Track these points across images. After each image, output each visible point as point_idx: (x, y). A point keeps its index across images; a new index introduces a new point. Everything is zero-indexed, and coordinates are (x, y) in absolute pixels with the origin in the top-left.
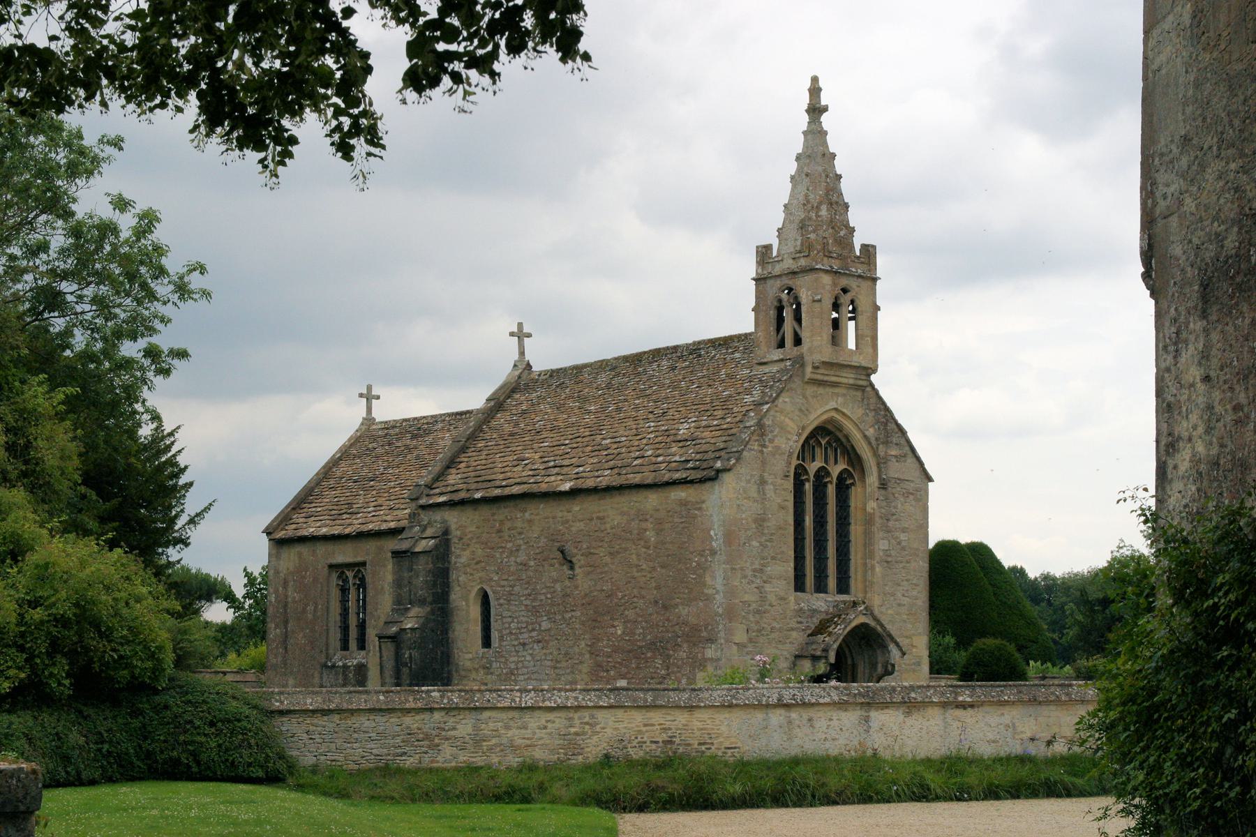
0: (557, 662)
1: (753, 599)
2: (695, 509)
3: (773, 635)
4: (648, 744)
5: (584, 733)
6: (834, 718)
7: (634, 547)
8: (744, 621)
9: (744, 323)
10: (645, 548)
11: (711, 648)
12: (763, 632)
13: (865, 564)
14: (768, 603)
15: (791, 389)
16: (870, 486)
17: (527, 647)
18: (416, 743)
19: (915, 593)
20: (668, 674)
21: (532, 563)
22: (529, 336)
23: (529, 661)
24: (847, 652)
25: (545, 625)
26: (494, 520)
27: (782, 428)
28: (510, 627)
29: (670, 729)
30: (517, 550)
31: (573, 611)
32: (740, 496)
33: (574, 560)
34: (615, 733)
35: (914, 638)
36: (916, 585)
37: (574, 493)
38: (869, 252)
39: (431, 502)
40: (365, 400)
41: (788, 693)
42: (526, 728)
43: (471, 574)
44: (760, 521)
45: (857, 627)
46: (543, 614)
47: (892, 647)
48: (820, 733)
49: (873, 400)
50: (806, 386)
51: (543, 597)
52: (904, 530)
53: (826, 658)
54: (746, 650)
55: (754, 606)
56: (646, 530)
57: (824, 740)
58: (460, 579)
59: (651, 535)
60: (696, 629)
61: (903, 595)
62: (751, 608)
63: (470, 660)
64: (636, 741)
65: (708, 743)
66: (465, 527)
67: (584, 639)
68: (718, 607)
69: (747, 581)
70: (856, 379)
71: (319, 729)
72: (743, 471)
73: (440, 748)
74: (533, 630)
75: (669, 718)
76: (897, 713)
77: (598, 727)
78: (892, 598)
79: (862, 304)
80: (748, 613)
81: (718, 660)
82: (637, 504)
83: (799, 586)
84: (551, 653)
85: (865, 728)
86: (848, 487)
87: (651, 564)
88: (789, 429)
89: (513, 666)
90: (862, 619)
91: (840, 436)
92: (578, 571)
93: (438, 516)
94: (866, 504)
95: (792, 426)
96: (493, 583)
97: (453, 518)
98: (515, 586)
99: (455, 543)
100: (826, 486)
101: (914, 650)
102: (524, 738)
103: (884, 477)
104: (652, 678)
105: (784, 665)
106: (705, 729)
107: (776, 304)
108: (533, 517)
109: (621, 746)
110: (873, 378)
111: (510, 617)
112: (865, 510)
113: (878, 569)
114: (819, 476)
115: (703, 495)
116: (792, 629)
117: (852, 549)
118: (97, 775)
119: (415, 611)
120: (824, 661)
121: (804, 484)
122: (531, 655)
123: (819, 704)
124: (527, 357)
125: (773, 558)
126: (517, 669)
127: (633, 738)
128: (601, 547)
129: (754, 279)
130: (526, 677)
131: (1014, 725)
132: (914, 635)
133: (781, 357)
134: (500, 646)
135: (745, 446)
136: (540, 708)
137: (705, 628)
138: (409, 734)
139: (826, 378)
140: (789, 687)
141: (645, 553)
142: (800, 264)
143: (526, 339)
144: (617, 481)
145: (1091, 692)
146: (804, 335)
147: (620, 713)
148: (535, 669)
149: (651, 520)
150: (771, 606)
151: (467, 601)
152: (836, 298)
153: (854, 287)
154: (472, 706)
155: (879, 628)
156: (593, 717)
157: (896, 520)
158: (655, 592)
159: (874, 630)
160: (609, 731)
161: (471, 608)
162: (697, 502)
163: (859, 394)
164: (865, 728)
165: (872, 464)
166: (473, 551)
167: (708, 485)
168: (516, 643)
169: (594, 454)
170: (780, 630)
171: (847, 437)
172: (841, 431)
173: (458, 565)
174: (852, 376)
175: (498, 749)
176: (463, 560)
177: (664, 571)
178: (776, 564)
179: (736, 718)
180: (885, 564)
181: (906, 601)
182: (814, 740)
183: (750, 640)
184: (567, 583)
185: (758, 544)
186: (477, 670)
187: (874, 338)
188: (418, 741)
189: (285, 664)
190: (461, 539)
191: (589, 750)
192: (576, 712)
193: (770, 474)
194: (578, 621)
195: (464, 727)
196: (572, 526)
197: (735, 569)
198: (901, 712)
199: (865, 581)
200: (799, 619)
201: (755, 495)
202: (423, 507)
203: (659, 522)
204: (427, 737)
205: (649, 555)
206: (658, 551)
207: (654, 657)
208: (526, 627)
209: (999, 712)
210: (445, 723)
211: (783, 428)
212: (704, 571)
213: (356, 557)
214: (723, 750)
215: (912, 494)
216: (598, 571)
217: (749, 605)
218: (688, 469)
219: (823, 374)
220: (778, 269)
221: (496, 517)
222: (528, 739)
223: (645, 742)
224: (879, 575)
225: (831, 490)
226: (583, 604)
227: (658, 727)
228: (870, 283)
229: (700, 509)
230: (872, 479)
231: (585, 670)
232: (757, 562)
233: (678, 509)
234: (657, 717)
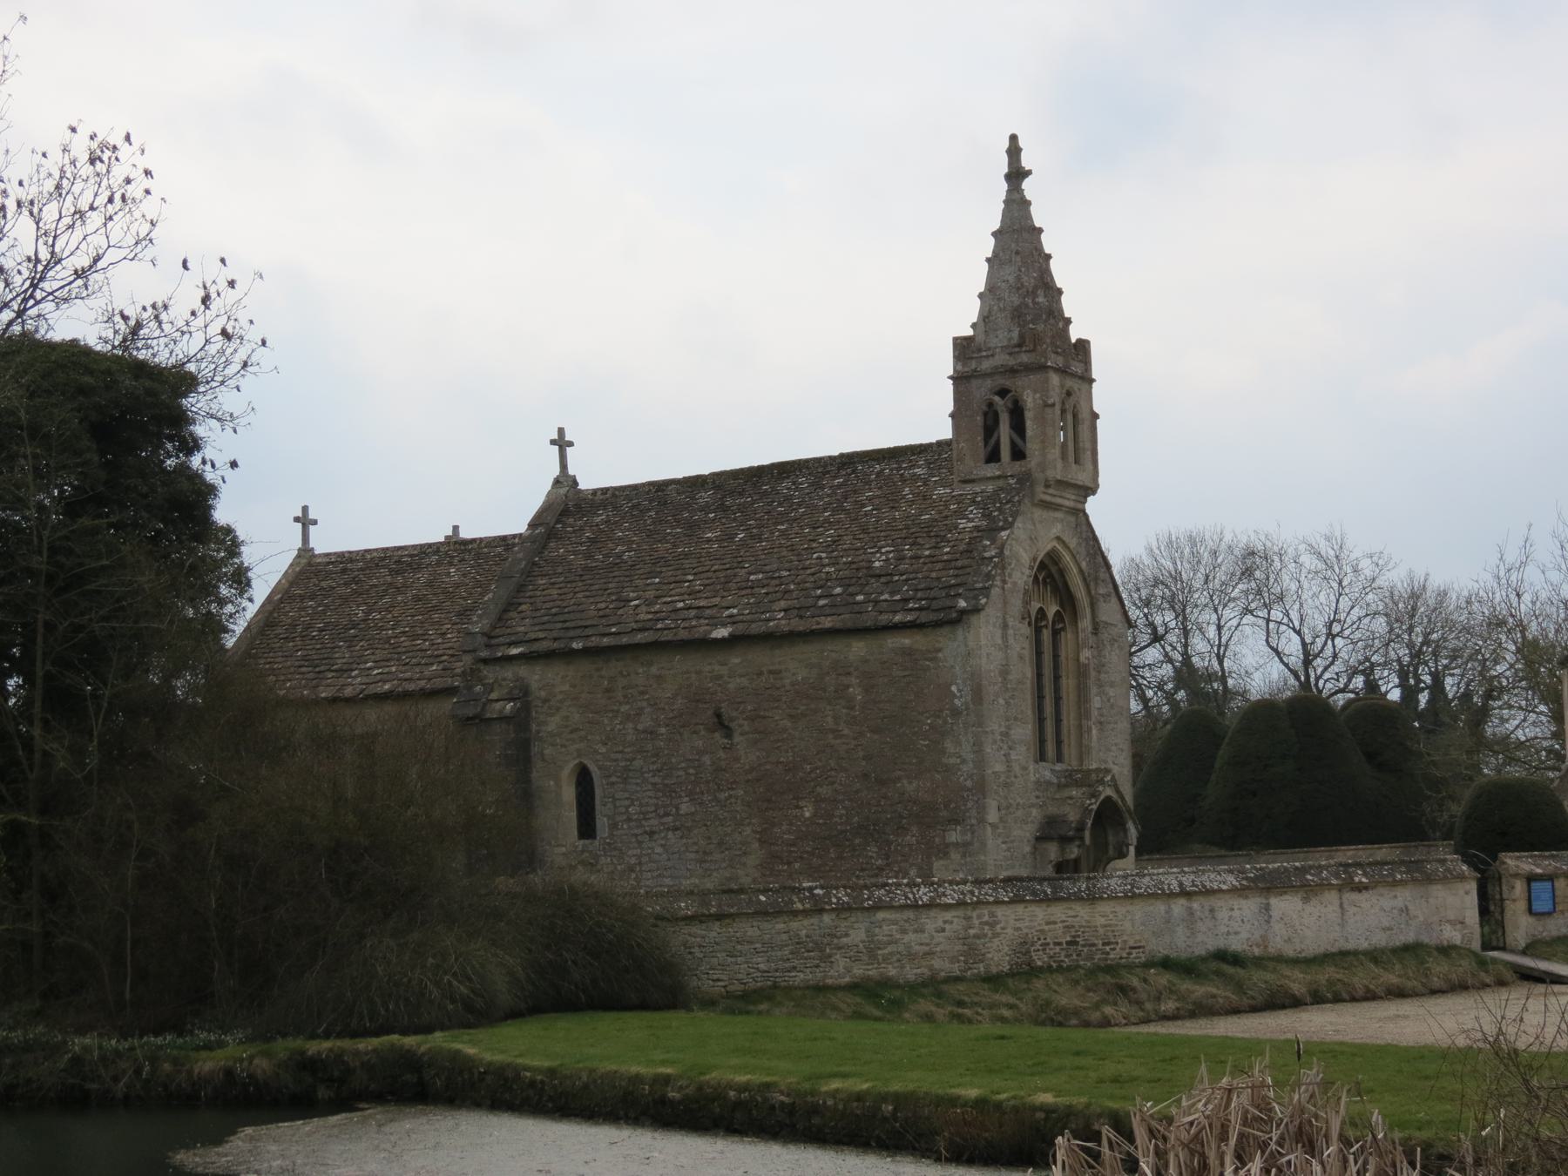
1: (1002, 770)
2: (926, 659)
4: (1052, 946)
5: (985, 935)
6: (1236, 907)
7: (828, 707)
9: (938, 428)
10: (848, 708)
11: (956, 830)
13: (1080, 726)
16: (1083, 630)
17: (656, 836)
18: (806, 955)
20: (888, 865)
21: (663, 730)
23: (660, 854)
26: (602, 677)
28: (627, 811)
29: (1073, 927)
31: (733, 789)
33: (732, 725)
34: (1016, 934)
38: (1083, 347)
39: (500, 654)
40: (300, 525)
42: (923, 931)
46: (683, 794)
51: (681, 773)
53: (1082, 839)
56: (848, 687)
58: (546, 752)
59: (857, 693)
64: (1040, 943)
65: (1112, 943)
66: (553, 685)
67: (749, 824)
71: (698, 939)
73: (833, 960)
74: (667, 814)
75: (1071, 913)
77: (998, 927)
81: (966, 844)
82: (833, 654)
83: (1042, 757)
84: (695, 844)
91: (1054, 569)
92: (737, 738)
93: (509, 673)
95: (1025, 558)
96: (599, 757)
97: (535, 677)
98: (634, 759)
99: (536, 706)
102: (922, 944)
104: (862, 870)
106: (1110, 925)
107: (985, 408)
109: (1024, 950)
111: (627, 799)
112: (1078, 660)
115: (937, 641)
116: (1033, 805)
118: (1420, 988)
120: (1077, 843)
122: (662, 845)
123: (1220, 891)
125: (1016, 719)
127: (1035, 939)
128: (777, 708)
129: (950, 377)
130: (655, 874)
131: (1406, 908)
133: (998, 473)
134: (611, 835)
137: (945, 806)
138: (798, 943)
140: (1185, 873)
142: (1019, 361)
147: (1020, 908)
148: (670, 864)
153: (1076, 389)
156: (992, 915)
158: (864, 763)
160: (1009, 931)
162: (929, 651)
163: (1072, 519)
164: (1266, 918)
167: (945, 630)
168: (639, 831)
169: (744, 592)
174: (1073, 497)
175: (895, 959)
177: (876, 737)
179: (1138, 910)
184: (722, 754)
188: (808, 951)
190: (546, 701)
191: (990, 956)
192: (974, 909)
194: (739, 801)
195: (857, 934)
199: (1080, 745)
202: (485, 661)
204: (819, 947)
205: (854, 717)
208: (655, 811)
214: (1127, 951)
219: (1051, 495)
220: (986, 365)
221: (603, 673)
223: (1048, 944)
225: (1046, 635)
226: (748, 781)
227: (1060, 925)
228: (1087, 386)
229: (931, 660)
230: (1085, 623)
234: (1059, 912)
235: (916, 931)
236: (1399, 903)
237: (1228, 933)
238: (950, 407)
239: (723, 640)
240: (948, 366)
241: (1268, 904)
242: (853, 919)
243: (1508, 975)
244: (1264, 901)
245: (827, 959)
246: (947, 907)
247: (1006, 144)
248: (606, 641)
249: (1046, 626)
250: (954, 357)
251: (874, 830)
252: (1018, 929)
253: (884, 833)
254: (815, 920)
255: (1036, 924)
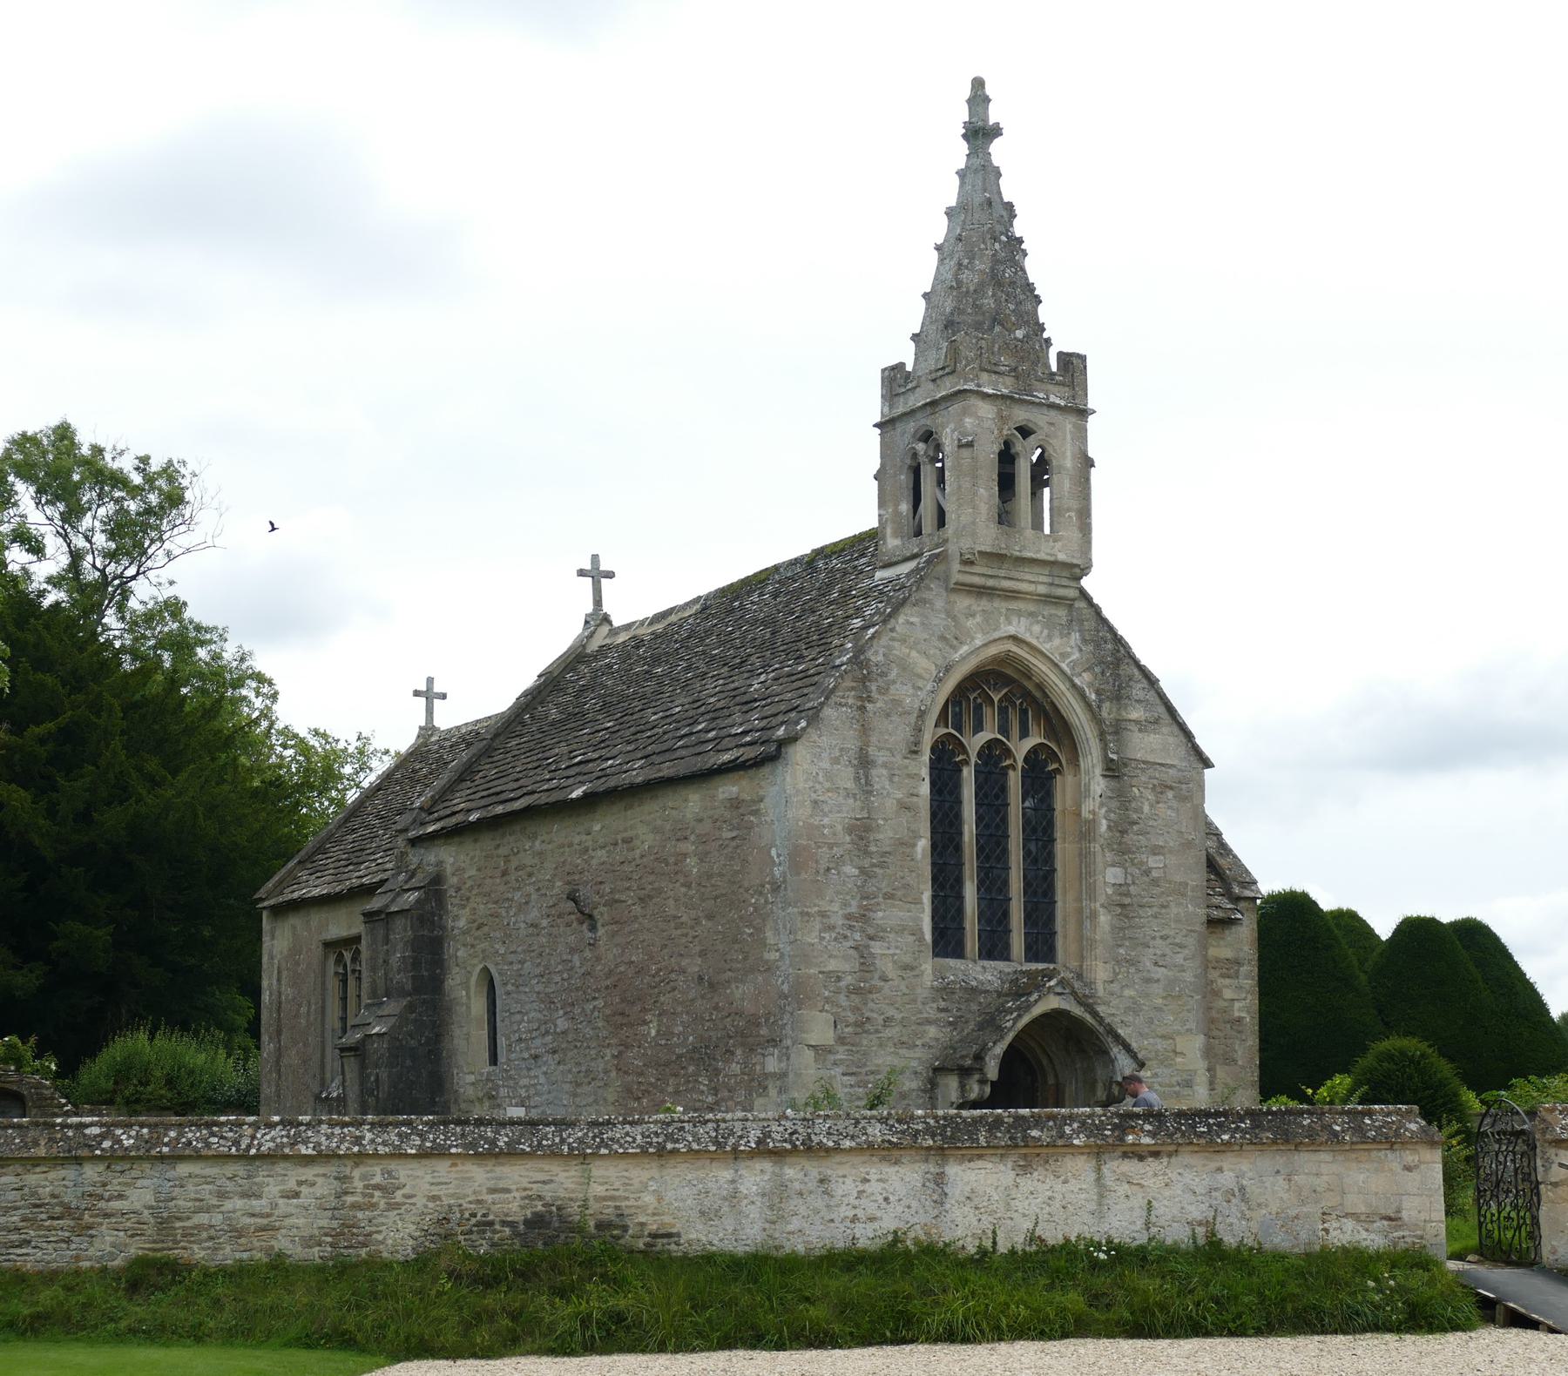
0: (578, 1085)
1: (847, 967)
3: (888, 1033)
4: (497, 1227)
5: (373, 1206)
6: (873, 1177)
8: (827, 1007)
11: (773, 1055)
12: (868, 1026)
14: (876, 976)
15: (924, 601)
18: (47, 1223)
19: (1179, 959)
20: (717, 1103)
21: (544, 923)
22: (610, 575)
24: (1045, 1062)
25: (562, 1024)
27: (904, 669)
30: (527, 903)
32: (818, 786)
34: (431, 1205)
35: (1178, 1039)
36: (1181, 946)
37: (590, 801)
38: (1073, 365)
40: (423, 700)
41: (781, 1129)
43: (473, 946)
44: (861, 830)
45: (1045, 1016)
47: (1116, 1051)
48: (843, 1208)
49: (1090, 624)
50: (954, 597)
52: (1156, 851)
54: (832, 1057)
55: (849, 979)
57: (852, 1221)
58: (459, 954)
60: (754, 1022)
61: (1156, 964)
62: (842, 984)
63: (473, 1084)
68: (783, 983)
69: (834, 935)
70: (1052, 584)
72: (825, 741)
73: (93, 1232)
74: (547, 1032)
76: (1002, 1167)
77: (399, 1193)
78: (1132, 970)
79: (1065, 460)
80: (837, 992)
82: (674, 812)
83: (947, 940)
85: (935, 1197)
86: (1051, 776)
87: (693, 913)
88: (920, 671)
89: (523, 1093)
90: (1052, 1003)
91: (1030, 686)
92: (601, 932)
94: (1080, 806)
95: (925, 665)
97: (448, 857)
99: (451, 896)
100: (1007, 774)
101: (1179, 1060)
103: (1114, 757)
105: (911, 1084)
106: (612, 1198)
108: (544, 846)
110: (1086, 583)
112: (1079, 815)
113: (1104, 919)
114: (990, 756)
115: (761, 787)
116: (929, 1022)
117: (1059, 885)
119: (393, 1007)
120: (977, 1077)
121: (961, 771)
122: (545, 1073)
124: (606, 608)
125: (889, 896)
126: (529, 1097)
128: (628, 889)
131: (1242, 1189)
132: (1179, 1033)
135: (827, 698)
136: (286, 1157)
139: (990, 583)
141: (685, 895)
143: (603, 581)
144: (653, 774)
145: (1413, 1127)
146: (949, 508)
147: (442, 1166)
149: (692, 838)
150: (885, 979)
151: (468, 989)
152: (1007, 444)
154: (153, 1153)
155: (1088, 1018)
157: (1140, 833)
159: (1077, 1022)
161: (473, 1001)
163: (1062, 613)
165: (1090, 735)
166: (475, 909)
167: (766, 770)
170: (904, 1023)
171: (1040, 687)
172: (1030, 678)
173: (456, 931)
174: (1046, 579)
175: (204, 1235)
176: (462, 923)
178: (894, 906)
180: (1119, 910)
181: (1160, 973)
182: (832, 1221)
183: (841, 1040)
184: (588, 954)
185: (856, 872)
186: (480, 1100)
187: (1084, 514)
188: (53, 1218)
189: (279, 1096)
192: (357, 1165)
193: (880, 749)
196: (593, 857)
197: (808, 914)
198: (1010, 1165)
199: (1080, 938)
200: (943, 1004)
201: (850, 785)
203: (703, 840)
206: (703, 890)
207: (697, 1074)
209: (1213, 1165)
210: (104, 1185)
211: (904, 667)
212: (764, 920)
213: (350, 927)
215: (1171, 788)
216: (627, 929)
217: (839, 979)
218: (742, 745)
222: (261, 1216)
224: (1107, 928)
227: (517, 1195)
229: (756, 813)
230: (1092, 759)
231: (611, 1098)
232: (854, 903)
233: (727, 815)
234: (517, 1175)
235: (245, 1195)
236: (1227, 1179)
237: (855, 1219)
238: (875, 464)
239: (578, 799)
240: (872, 407)
241: (942, 1175)
242: (134, 1173)
243: (1469, 1308)
244: (933, 1169)
245: (84, 1230)
246: (307, 1160)
247: (967, 93)
248: (500, 809)
249: (966, 762)
250: (882, 396)
251: (706, 1053)
252: (434, 1198)
253: (714, 1059)
254: (70, 1173)
255: (470, 1191)
